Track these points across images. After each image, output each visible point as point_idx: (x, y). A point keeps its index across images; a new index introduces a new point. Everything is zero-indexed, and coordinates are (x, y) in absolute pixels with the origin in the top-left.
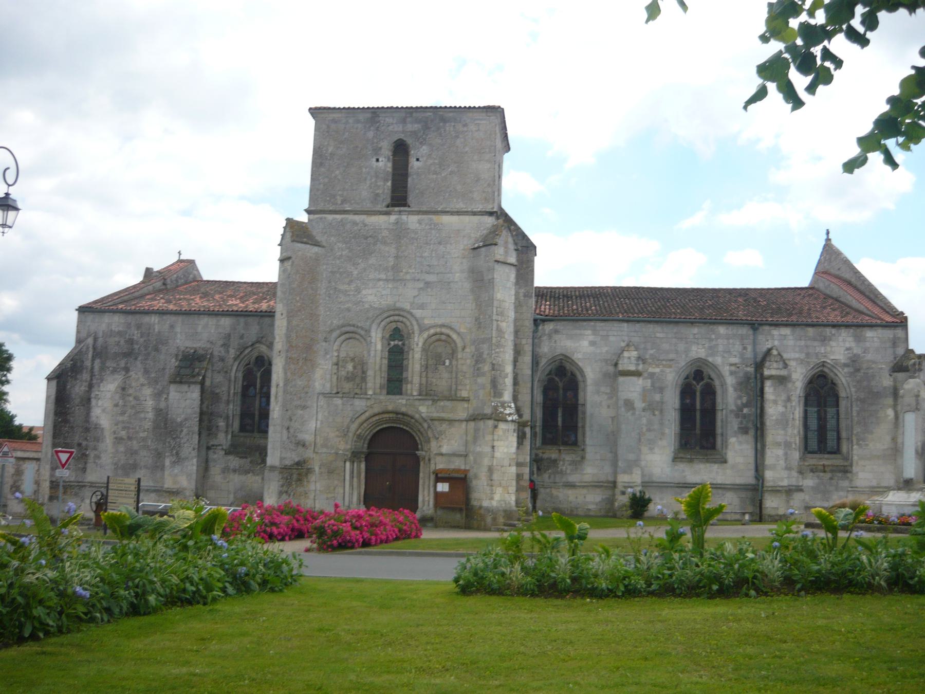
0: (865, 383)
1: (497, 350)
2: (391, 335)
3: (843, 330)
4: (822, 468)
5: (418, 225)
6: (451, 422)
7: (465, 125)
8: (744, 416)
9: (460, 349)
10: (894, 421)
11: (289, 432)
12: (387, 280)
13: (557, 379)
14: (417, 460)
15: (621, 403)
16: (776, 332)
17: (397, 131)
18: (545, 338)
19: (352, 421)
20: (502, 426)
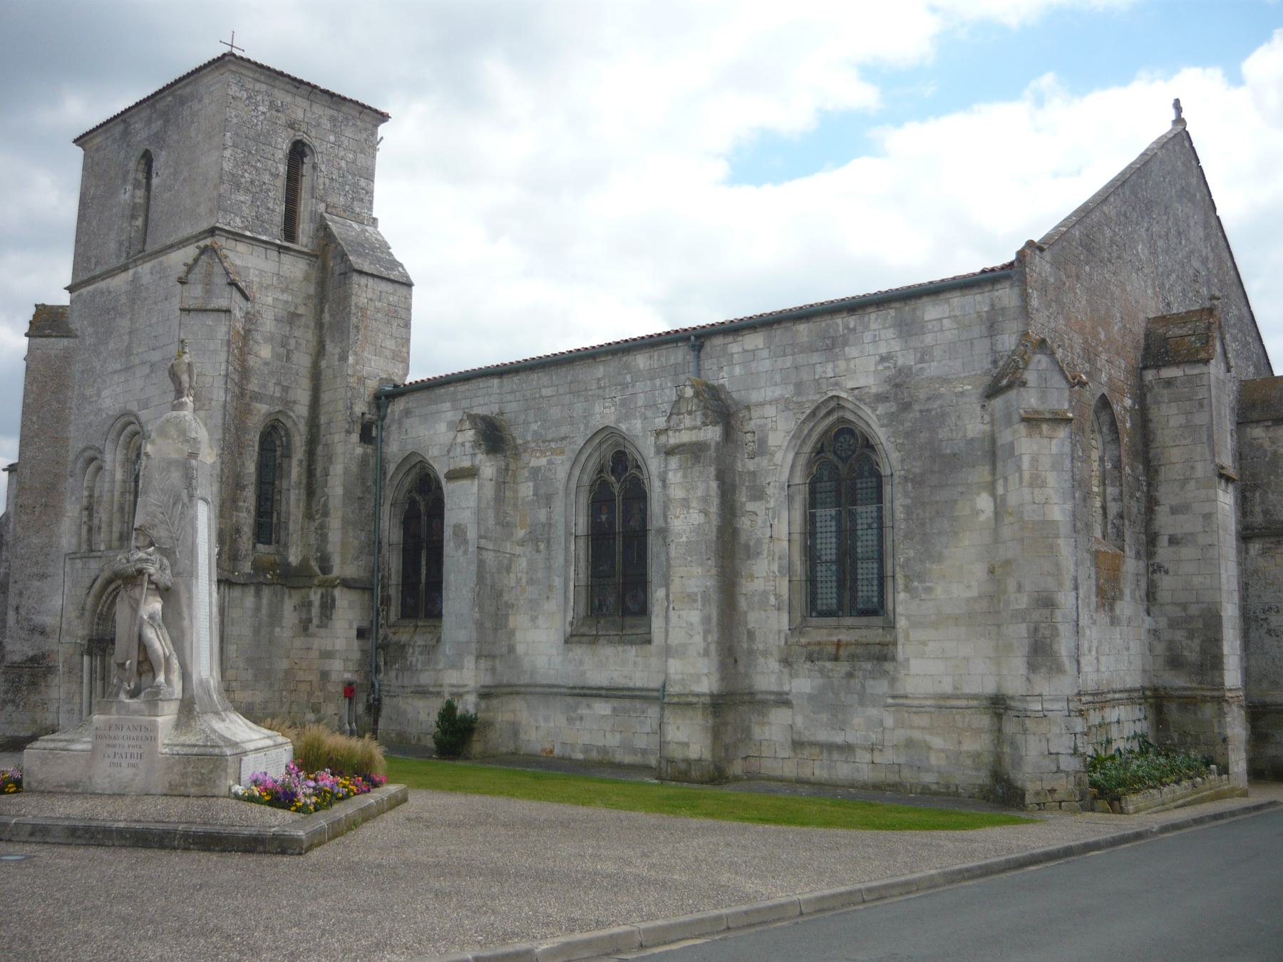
0: (923, 437)
3: (873, 316)
11: (18, 613)
12: (120, 371)
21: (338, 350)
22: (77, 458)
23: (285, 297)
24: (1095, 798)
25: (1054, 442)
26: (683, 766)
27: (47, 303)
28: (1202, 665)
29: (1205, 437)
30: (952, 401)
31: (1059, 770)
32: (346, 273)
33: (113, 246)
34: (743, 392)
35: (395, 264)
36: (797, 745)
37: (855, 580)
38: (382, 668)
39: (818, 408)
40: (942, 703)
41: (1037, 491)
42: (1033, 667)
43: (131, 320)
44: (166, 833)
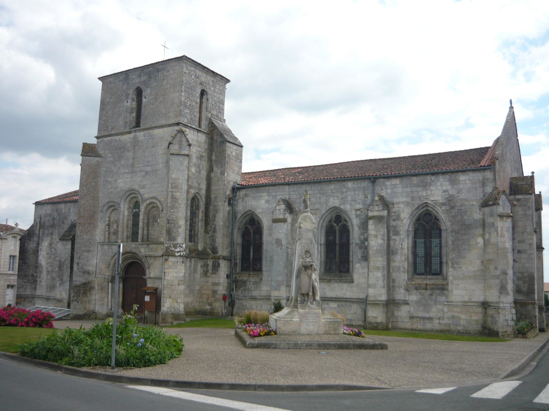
0: (459, 218)
1: (172, 211)
2: (134, 206)
3: (441, 177)
4: (424, 286)
5: (143, 137)
6: (155, 257)
10: (483, 247)
12: (128, 173)
13: (250, 227)
16: (388, 183)
17: (136, 81)
19: (112, 259)
20: (171, 259)
21: (220, 171)
22: (104, 206)
23: (199, 149)
24: (518, 334)
25: (507, 223)
26: (376, 325)
27: (87, 143)
28: (528, 292)
29: (530, 219)
30: (469, 207)
31: (508, 325)
32: (223, 142)
33: (121, 123)
34: (391, 199)
35: (236, 139)
36: (412, 317)
37: (431, 263)
38: (234, 289)
39: (419, 206)
40: (464, 304)
41: (502, 238)
42: (501, 293)
43: (134, 153)
44: (348, 344)
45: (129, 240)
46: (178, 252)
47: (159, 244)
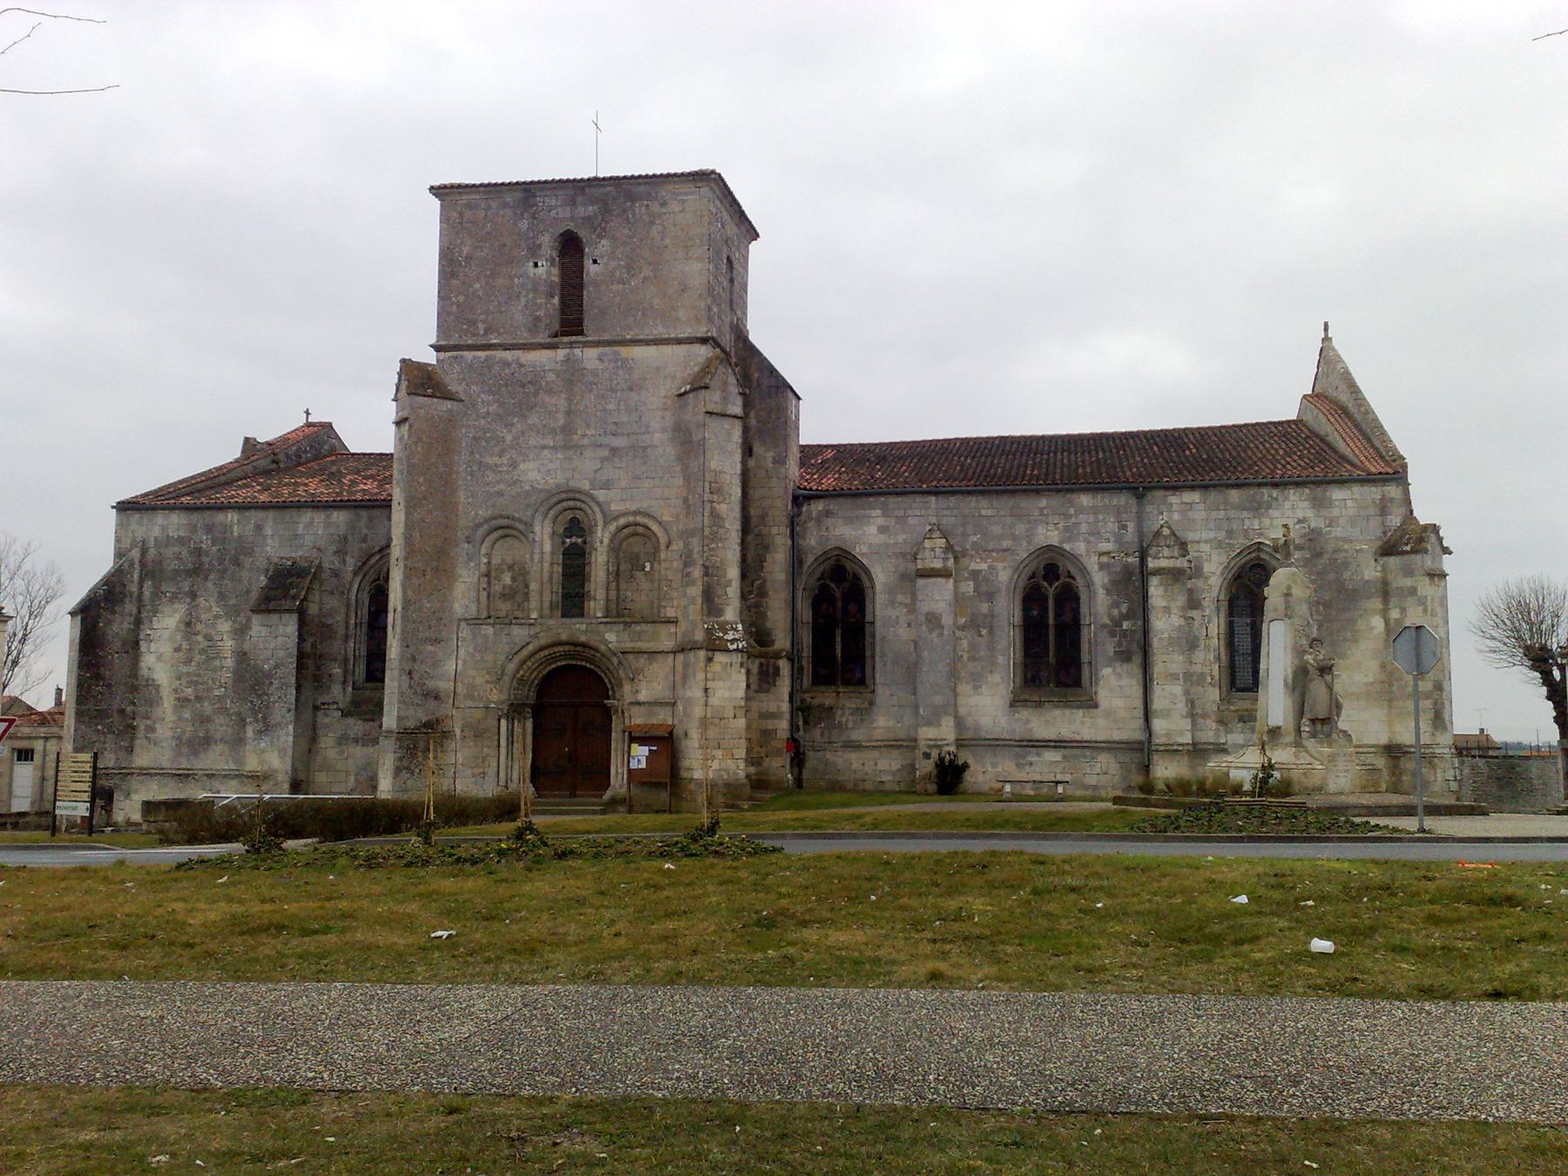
0: (1332, 576)
3: (1292, 491)
5: (597, 362)
6: (653, 654)
7: (663, 204)
8: (1124, 634)
9: (663, 547)
10: (1383, 635)
11: (411, 678)
12: (554, 448)
13: (832, 585)
14: (607, 713)
15: (922, 618)
16: (1174, 499)
17: (562, 216)
18: (810, 525)
20: (720, 658)
45: (555, 612)
46: (732, 641)
47: (664, 622)
